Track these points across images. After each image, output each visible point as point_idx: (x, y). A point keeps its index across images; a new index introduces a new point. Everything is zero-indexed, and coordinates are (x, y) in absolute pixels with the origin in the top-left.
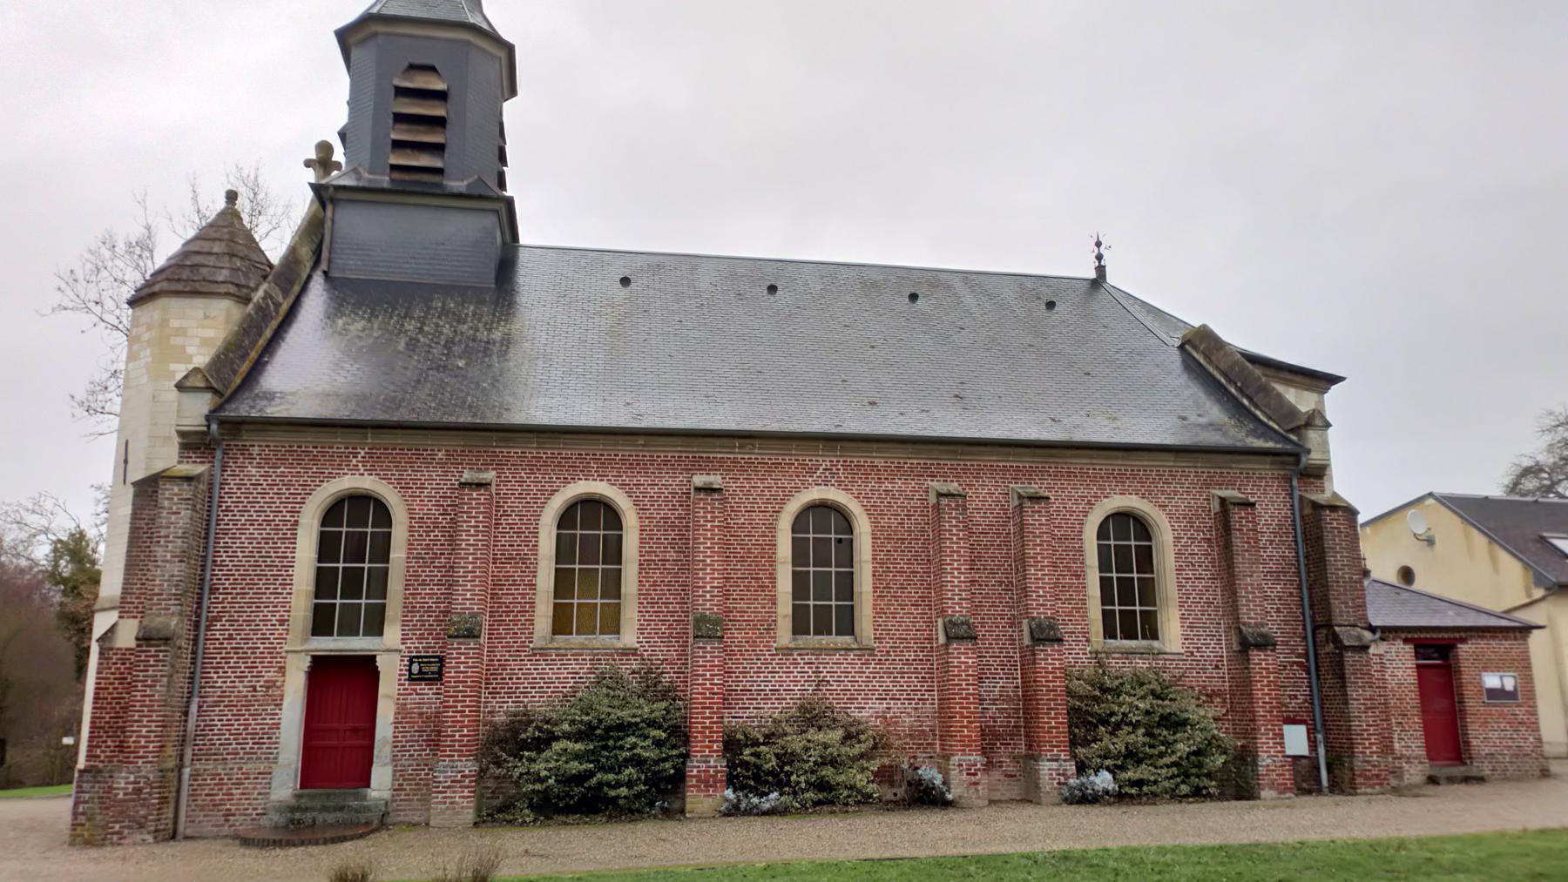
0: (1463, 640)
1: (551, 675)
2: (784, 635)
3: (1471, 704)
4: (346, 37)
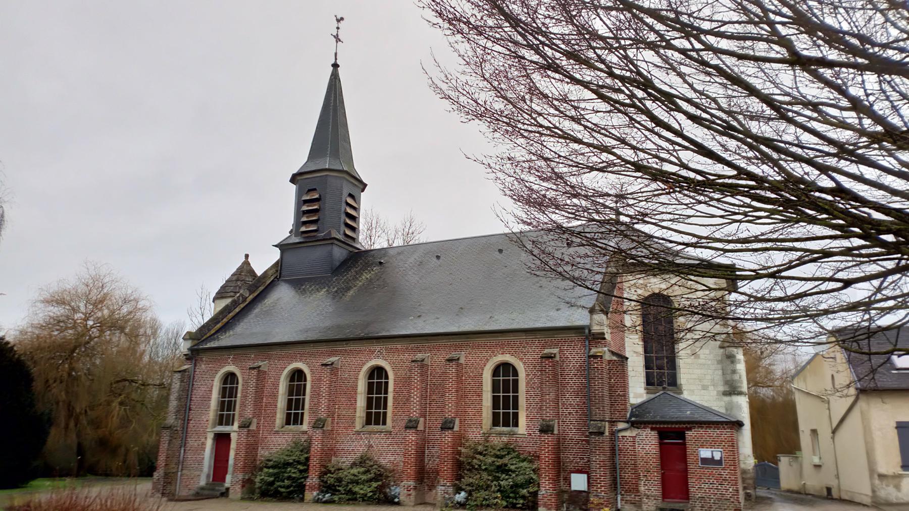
0: (690, 429)
1: (278, 442)
2: (358, 426)
3: (693, 468)
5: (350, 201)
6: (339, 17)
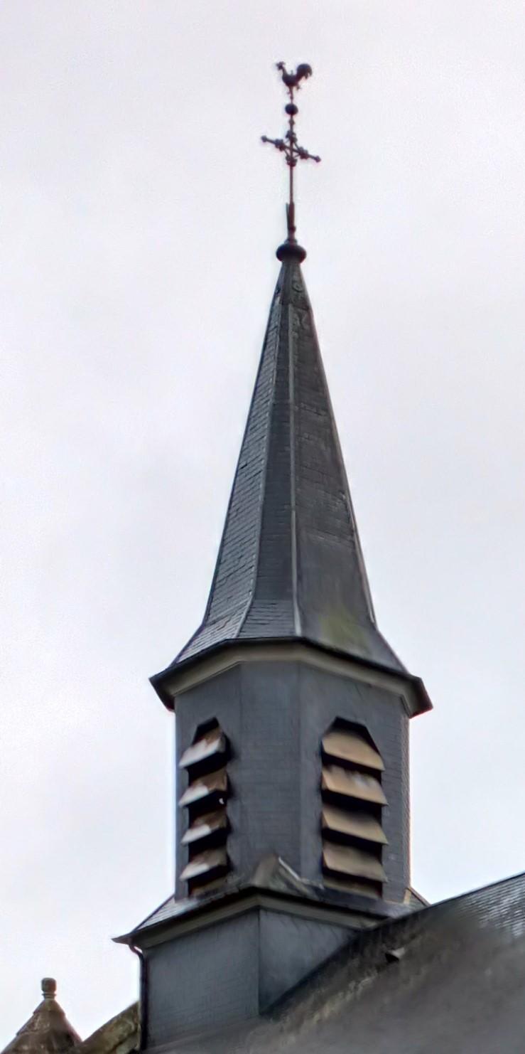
4: (164, 684)
5: (338, 746)
6: (291, 69)
